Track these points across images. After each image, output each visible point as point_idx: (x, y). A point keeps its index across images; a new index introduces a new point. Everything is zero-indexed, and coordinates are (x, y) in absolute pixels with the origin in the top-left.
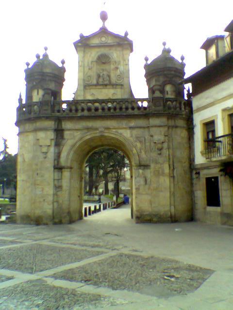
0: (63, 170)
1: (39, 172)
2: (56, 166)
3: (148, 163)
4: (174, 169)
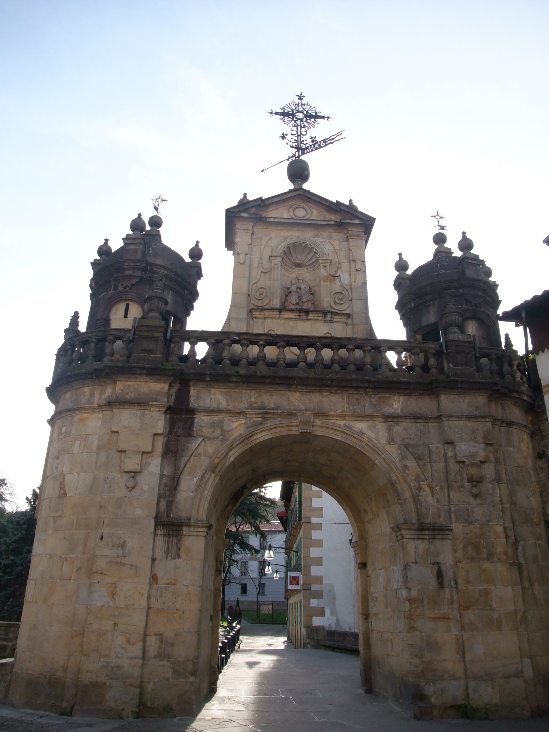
0: (346, 243)
1: (106, 531)
2: (165, 518)
3: (442, 520)
4: (516, 542)
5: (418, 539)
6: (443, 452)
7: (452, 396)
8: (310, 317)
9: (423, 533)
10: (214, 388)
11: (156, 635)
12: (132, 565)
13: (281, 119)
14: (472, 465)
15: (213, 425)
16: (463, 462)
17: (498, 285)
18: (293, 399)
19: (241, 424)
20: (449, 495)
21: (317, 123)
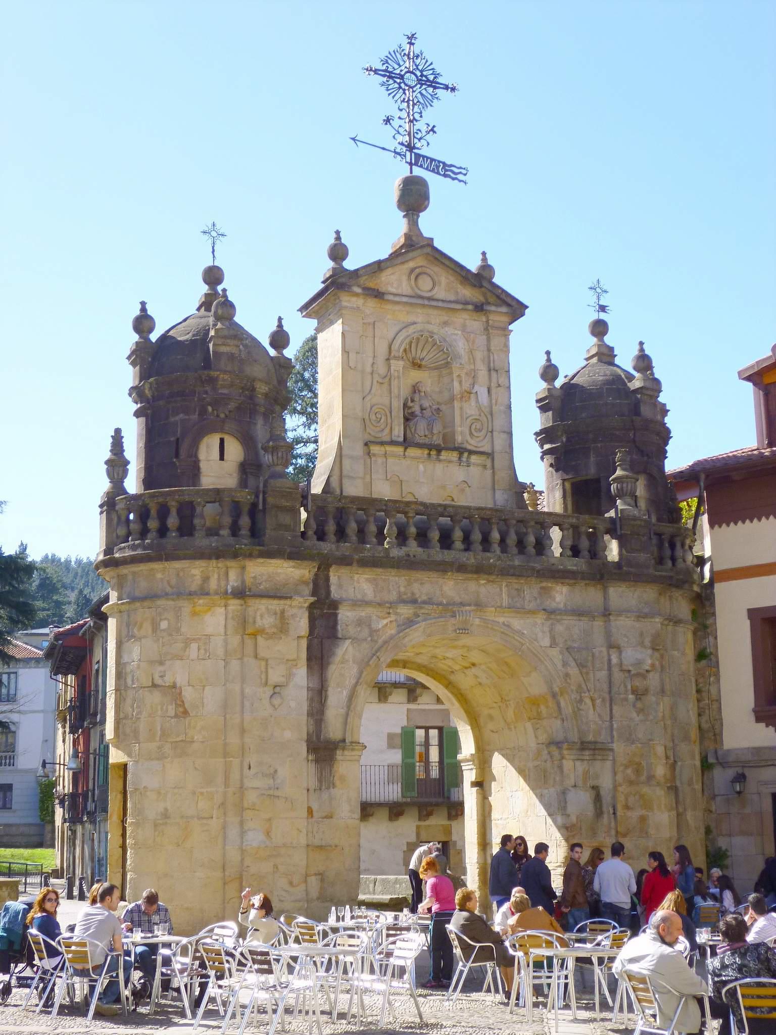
3: (603, 737)
5: (578, 759)
6: (606, 659)
7: (621, 589)
8: (441, 457)
9: (584, 753)
10: (357, 573)
11: (316, 874)
12: (286, 798)
13: (383, 84)
14: (638, 675)
15: (360, 623)
16: (629, 671)
17: (668, 411)
18: (446, 588)
19: (391, 622)
20: (611, 710)
21: (437, 98)
